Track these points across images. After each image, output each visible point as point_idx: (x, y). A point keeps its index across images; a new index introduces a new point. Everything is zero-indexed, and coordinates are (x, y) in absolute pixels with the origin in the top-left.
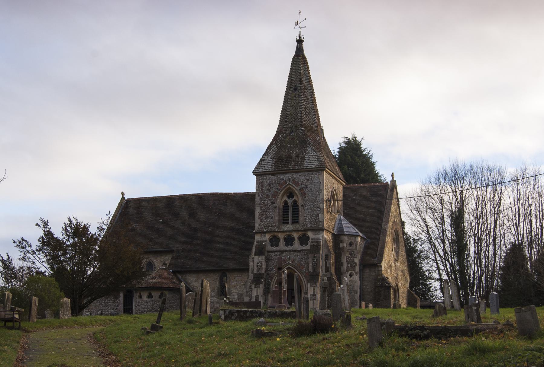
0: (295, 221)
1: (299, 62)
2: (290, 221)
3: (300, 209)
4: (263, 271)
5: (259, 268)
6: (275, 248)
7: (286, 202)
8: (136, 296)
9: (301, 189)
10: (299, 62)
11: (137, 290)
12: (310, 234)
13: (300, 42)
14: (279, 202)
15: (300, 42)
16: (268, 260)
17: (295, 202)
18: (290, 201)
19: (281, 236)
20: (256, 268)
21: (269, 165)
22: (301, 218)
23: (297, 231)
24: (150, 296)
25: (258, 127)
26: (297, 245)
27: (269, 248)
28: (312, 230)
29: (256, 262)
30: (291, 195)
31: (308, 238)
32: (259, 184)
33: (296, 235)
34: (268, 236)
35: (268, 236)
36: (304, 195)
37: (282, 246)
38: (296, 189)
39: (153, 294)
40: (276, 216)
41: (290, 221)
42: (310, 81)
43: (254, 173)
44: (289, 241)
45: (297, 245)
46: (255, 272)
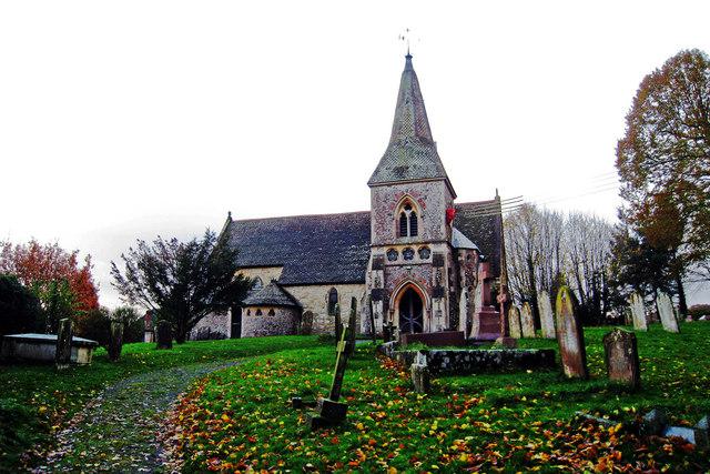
0: (414, 233)
1: (409, 72)
2: (409, 234)
3: (419, 220)
4: (382, 287)
5: (377, 284)
6: (410, 262)
7: (403, 214)
8: (244, 312)
9: (420, 201)
10: (409, 72)
11: (245, 306)
12: (431, 246)
13: (409, 57)
14: (397, 215)
15: (409, 57)
16: (386, 275)
17: (413, 214)
18: (408, 213)
19: (400, 249)
20: (373, 284)
21: (386, 175)
22: (420, 230)
23: (417, 244)
24: (259, 313)
25: (374, 138)
26: (417, 259)
27: (388, 263)
28: (434, 242)
29: (373, 276)
30: (408, 207)
31: (429, 251)
32: (376, 199)
33: (415, 248)
34: (385, 249)
35: (385, 249)
36: (423, 206)
37: (401, 260)
38: (414, 201)
39: (276, 311)
40: (393, 229)
41: (409, 234)
42: (309, 217)
43: (371, 184)
44: (408, 253)
45: (417, 259)
46: (373, 287)
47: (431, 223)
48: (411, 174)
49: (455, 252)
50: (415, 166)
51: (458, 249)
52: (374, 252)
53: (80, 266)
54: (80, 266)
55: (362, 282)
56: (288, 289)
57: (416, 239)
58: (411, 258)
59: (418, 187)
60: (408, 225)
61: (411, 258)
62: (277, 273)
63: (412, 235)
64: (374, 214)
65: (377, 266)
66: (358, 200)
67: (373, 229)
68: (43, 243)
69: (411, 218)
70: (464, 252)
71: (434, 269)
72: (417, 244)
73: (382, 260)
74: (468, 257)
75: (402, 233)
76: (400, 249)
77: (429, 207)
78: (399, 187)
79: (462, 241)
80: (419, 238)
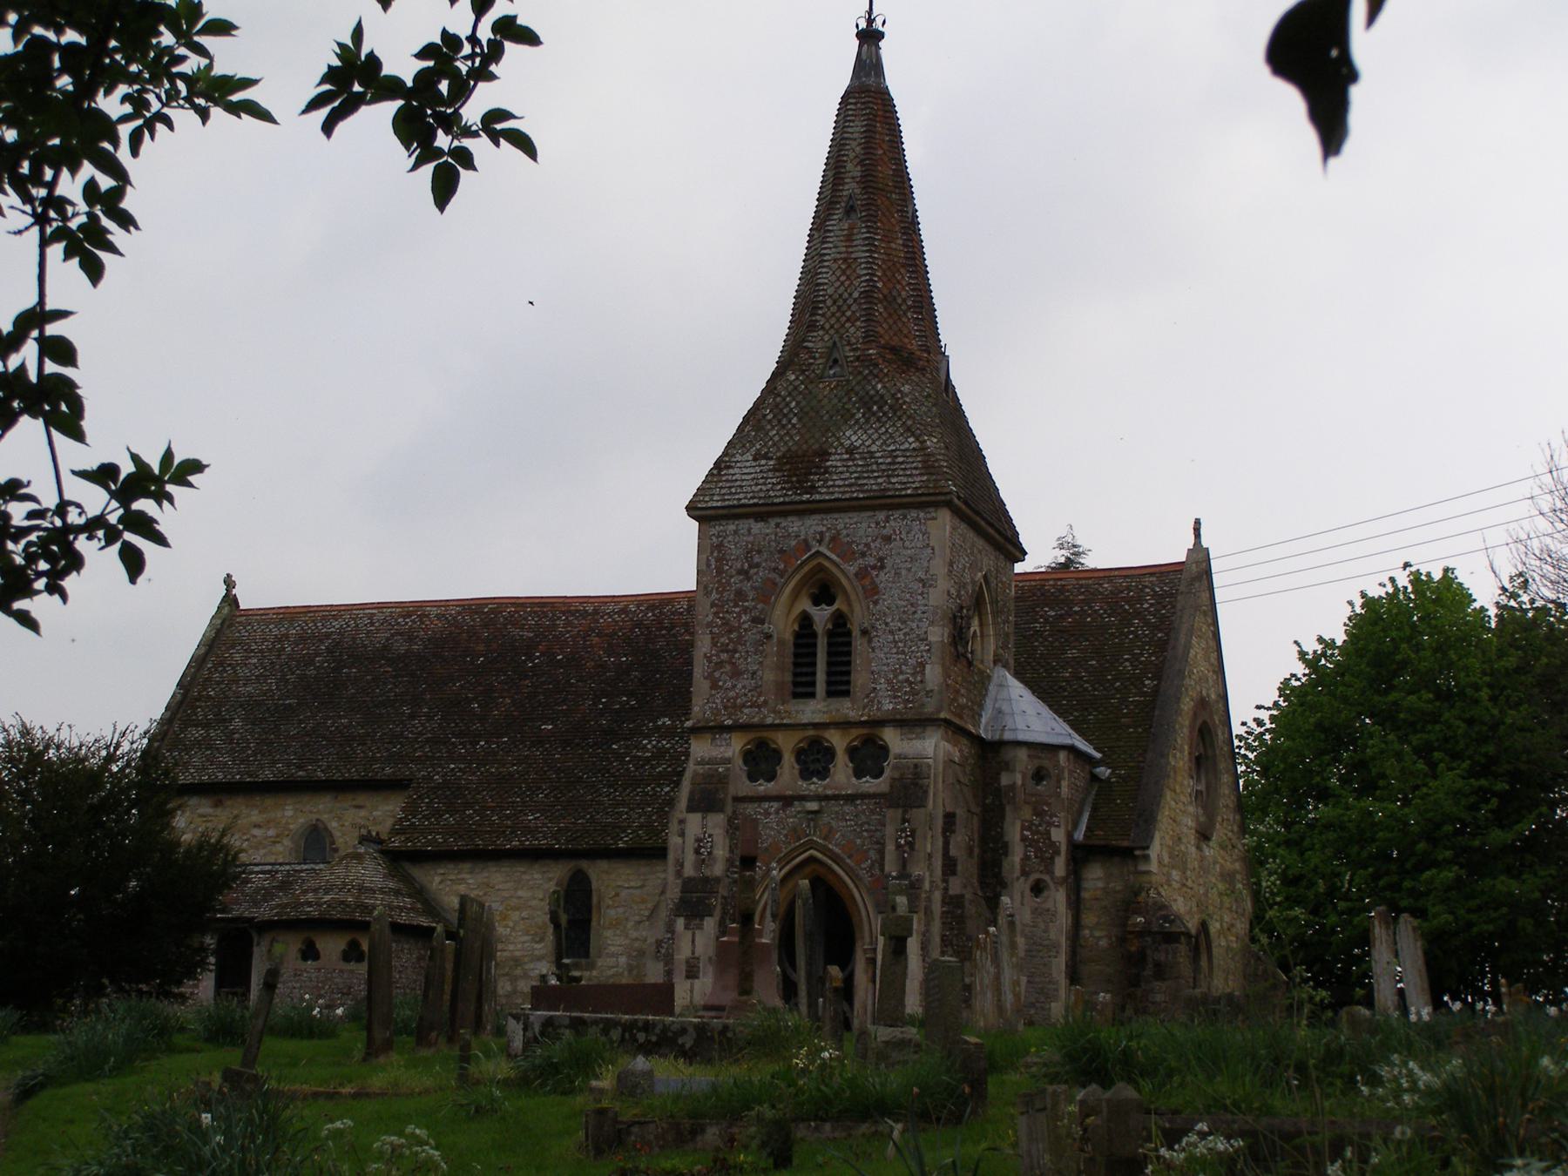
0: (839, 686)
6: (816, 786)
7: (805, 620)
9: (862, 574)
12: (890, 736)
13: (870, 37)
14: (782, 624)
15: (870, 37)
18: (821, 616)
19: (786, 743)
20: (690, 858)
22: (859, 679)
26: (842, 774)
29: (697, 838)
30: (824, 592)
32: (711, 558)
34: (734, 747)
36: (873, 592)
37: (788, 776)
40: (770, 670)
43: (692, 509)
44: (815, 758)
45: (842, 774)
47: (900, 648)
48: (838, 481)
49: (990, 754)
50: (851, 451)
51: (999, 745)
52: (701, 749)
53: (1403, 580)
54: (1403, 580)
55: (658, 853)
56: (418, 873)
57: (846, 709)
58: (823, 774)
59: (860, 527)
60: (823, 657)
61: (823, 774)
62: (383, 813)
63: (830, 694)
64: (705, 613)
65: (706, 801)
66: (652, 554)
67: (699, 670)
68: (35, 720)
69: (830, 634)
70: (1022, 754)
71: (893, 815)
72: (844, 725)
73: (723, 780)
74: (1039, 776)
75: (802, 689)
76: (788, 768)
77: (891, 598)
78: (794, 525)
79: (1026, 716)
80: (846, 709)
